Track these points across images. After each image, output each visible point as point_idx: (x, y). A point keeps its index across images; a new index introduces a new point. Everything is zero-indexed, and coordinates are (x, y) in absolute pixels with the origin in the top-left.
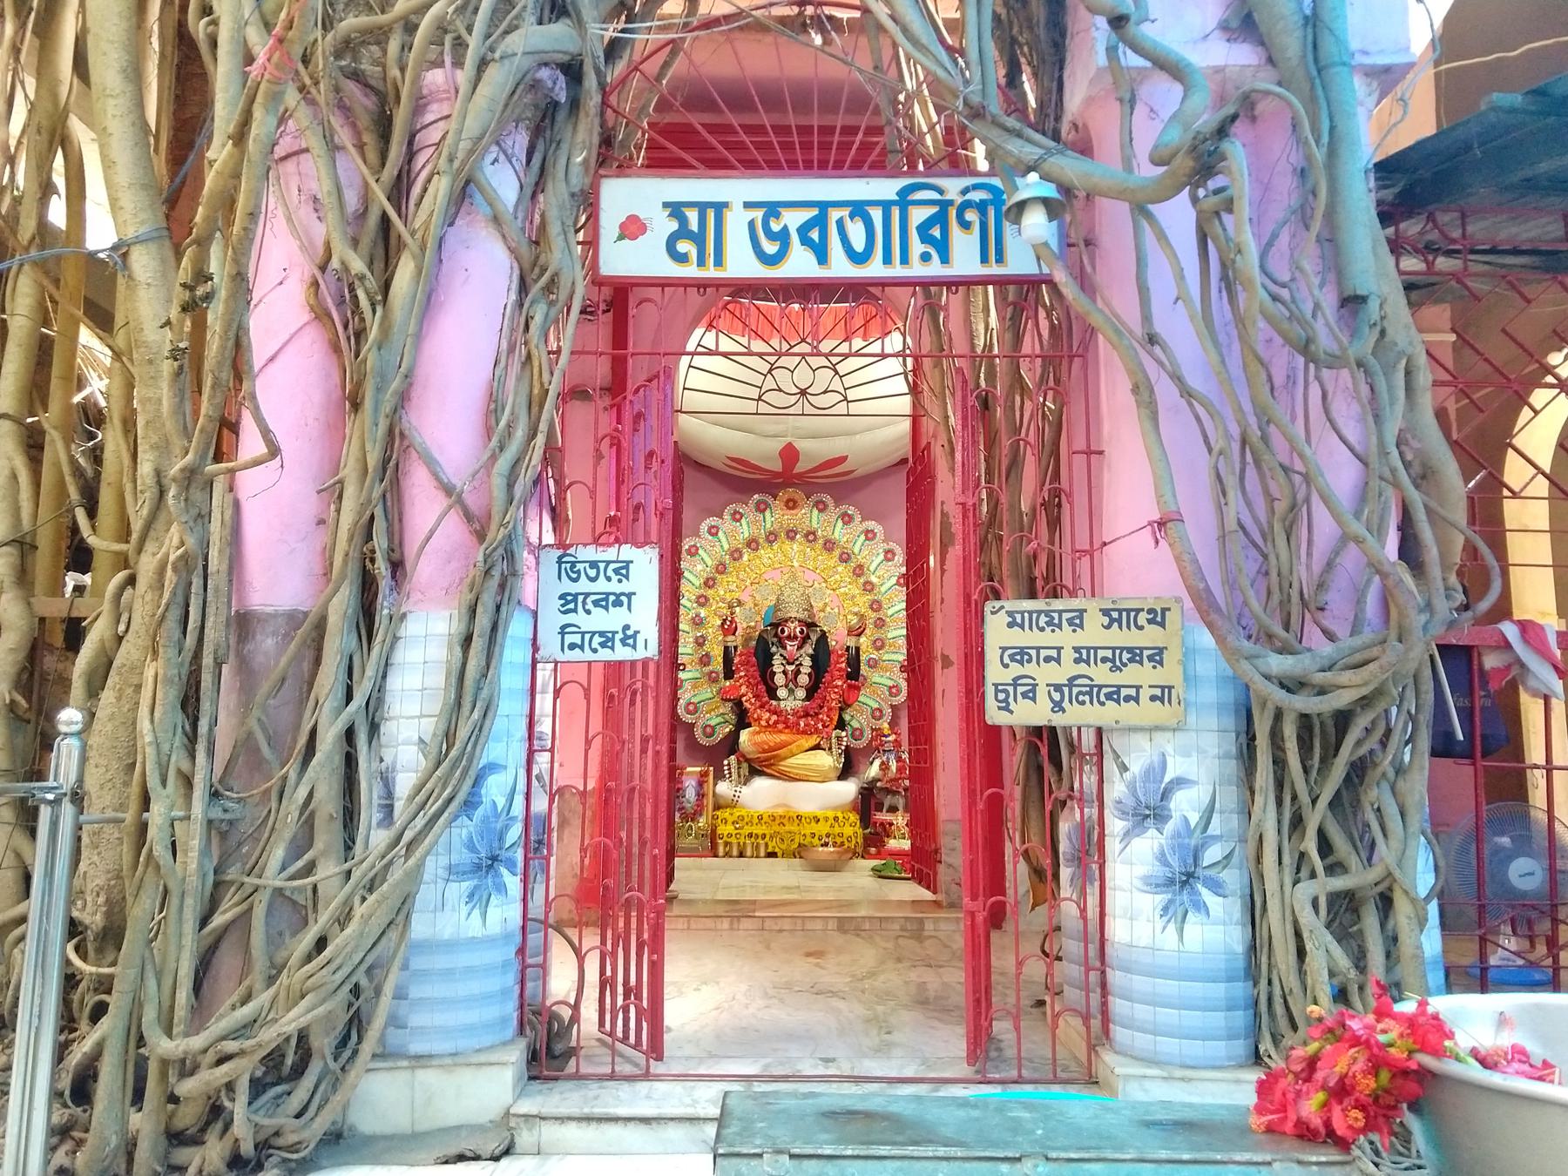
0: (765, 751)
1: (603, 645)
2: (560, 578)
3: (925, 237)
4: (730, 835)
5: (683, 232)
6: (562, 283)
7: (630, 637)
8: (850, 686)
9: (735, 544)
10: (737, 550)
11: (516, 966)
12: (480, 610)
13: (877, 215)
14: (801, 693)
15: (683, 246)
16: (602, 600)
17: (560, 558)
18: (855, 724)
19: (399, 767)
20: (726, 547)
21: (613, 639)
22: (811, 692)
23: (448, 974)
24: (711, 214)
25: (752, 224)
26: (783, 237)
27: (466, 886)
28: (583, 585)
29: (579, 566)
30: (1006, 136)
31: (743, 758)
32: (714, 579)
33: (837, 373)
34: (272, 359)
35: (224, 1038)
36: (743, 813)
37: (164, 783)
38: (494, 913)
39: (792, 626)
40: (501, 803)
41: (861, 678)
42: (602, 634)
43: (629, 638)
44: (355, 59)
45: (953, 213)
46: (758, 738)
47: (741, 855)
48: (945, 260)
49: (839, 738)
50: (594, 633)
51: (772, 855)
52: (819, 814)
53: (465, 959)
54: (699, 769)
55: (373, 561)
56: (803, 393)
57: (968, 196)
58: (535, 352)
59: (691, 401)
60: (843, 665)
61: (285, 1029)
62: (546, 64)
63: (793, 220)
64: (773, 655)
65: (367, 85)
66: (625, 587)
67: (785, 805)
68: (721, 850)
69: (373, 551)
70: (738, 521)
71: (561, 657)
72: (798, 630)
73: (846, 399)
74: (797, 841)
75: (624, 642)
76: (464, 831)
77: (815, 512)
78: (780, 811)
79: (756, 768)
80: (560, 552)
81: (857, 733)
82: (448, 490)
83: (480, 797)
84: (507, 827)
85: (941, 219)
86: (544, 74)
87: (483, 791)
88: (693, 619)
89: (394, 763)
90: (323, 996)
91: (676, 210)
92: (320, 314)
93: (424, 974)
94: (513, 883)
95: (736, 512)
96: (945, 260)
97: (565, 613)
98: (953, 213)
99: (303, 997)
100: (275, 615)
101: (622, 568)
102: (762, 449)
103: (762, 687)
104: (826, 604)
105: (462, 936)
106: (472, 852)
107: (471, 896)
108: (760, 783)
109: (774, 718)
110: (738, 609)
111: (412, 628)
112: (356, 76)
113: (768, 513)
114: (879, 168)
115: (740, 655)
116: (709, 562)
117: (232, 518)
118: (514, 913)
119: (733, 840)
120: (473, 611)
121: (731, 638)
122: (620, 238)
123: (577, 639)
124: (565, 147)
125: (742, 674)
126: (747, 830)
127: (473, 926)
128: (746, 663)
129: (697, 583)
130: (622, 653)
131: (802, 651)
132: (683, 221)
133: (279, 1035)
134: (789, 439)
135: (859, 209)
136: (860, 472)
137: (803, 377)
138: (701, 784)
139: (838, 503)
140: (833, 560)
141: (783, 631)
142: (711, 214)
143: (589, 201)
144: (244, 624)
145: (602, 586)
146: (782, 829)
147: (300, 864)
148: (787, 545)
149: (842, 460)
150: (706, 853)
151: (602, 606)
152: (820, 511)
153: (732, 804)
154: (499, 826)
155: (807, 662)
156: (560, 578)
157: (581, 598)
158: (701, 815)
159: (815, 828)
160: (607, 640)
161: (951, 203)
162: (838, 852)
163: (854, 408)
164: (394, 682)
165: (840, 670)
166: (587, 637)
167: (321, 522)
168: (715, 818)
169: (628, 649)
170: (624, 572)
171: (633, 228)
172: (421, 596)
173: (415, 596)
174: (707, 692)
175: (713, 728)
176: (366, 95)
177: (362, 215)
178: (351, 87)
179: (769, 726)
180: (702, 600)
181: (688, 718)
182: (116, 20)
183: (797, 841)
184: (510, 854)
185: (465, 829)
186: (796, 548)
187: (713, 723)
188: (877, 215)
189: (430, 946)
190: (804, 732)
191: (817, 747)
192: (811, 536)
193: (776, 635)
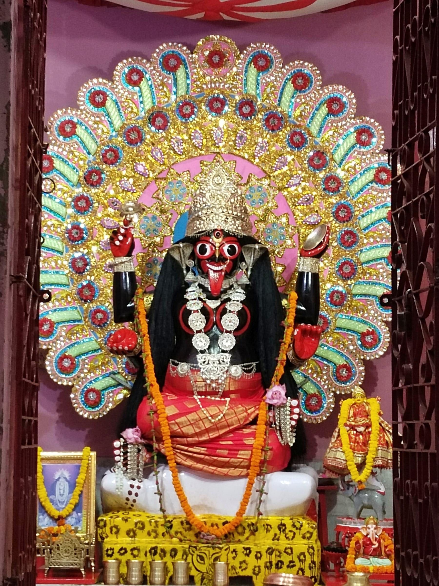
10: (135, 129)
20: (118, 123)
32: (99, 172)
64: (188, 285)
70: (136, 84)
72: (226, 247)
116: (92, 147)
131: (232, 280)
141: (203, 250)
180: (82, 204)
187: (98, 386)
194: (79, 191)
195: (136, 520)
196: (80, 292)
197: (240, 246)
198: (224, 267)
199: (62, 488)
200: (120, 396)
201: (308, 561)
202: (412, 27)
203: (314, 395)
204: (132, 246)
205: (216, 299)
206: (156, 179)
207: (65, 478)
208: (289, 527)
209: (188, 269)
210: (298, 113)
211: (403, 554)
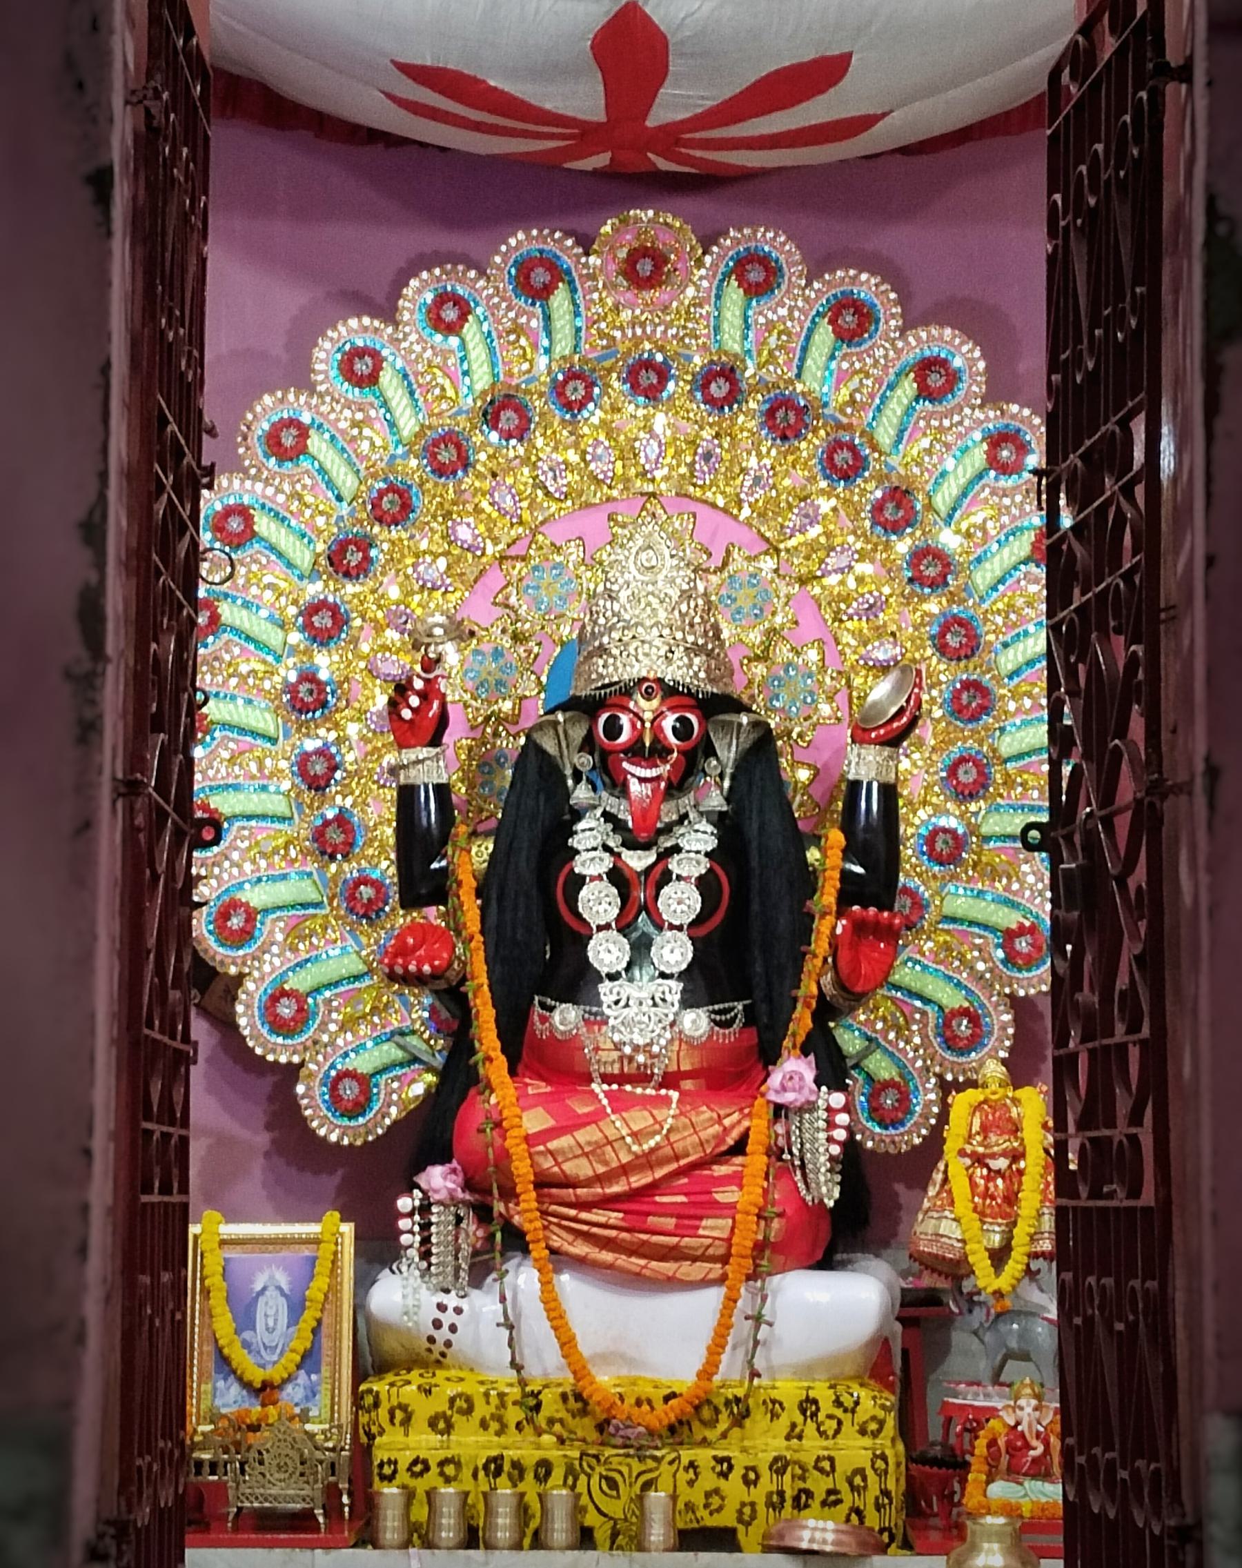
10: (451, 439)
20: (408, 425)
32: (365, 544)
47: (472, 1538)
64: (577, 815)
70: (451, 329)
72: (669, 722)
113: (560, 299)
116: (347, 481)
131: (686, 802)
141: (613, 729)
175: (364, 1081)
181: (281, 1050)
187: (363, 1063)
194: (314, 590)
195: (451, 1390)
196: (319, 835)
198: (663, 769)
199: (271, 1312)
200: (418, 1089)
202: (1088, 170)
204: (443, 721)
205: (646, 847)
207: (279, 1288)
208: (826, 1407)
209: (577, 776)
210: (844, 394)
211: (1081, 1460)
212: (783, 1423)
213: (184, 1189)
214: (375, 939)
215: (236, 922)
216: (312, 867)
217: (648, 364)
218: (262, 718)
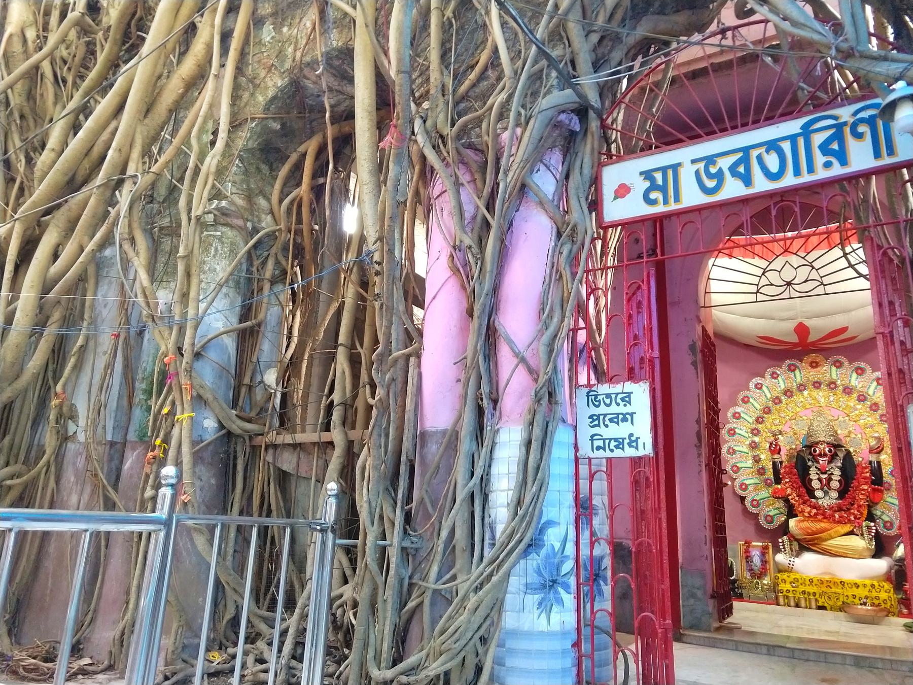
0: (809, 534)
1: (617, 447)
2: (588, 406)
3: (825, 148)
4: (788, 591)
5: (654, 187)
6: (579, 231)
7: (633, 441)
8: (874, 490)
9: (775, 394)
10: (777, 398)
11: (573, 654)
12: (535, 424)
13: (786, 146)
14: (835, 494)
15: (653, 195)
16: (615, 418)
17: (588, 393)
18: (886, 518)
19: (498, 520)
20: (769, 396)
21: (623, 443)
22: (842, 493)
23: (528, 653)
24: (670, 173)
25: (697, 173)
26: (720, 175)
27: (537, 597)
28: (603, 409)
29: (600, 397)
30: (874, 62)
31: (792, 538)
32: (762, 418)
33: (813, 268)
34: (434, 298)
35: (402, 674)
36: (798, 576)
37: (373, 524)
38: (556, 617)
39: (822, 447)
40: (557, 546)
41: (886, 485)
42: (616, 440)
43: (633, 442)
44: (469, 138)
45: (847, 130)
46: (804, 525)
47: (797, 605)
48: (844, 162)
49: (869, 527)
50: (610, 439)
51: (823, 608)
52: (858, 581)
53: (537, 645)
54: (761, 544)
55: (482, 399)
56: (789, 284)
57: (860, 115)
58: (564, 273)
59: (715, 299)
60: (868, 475)
61: (429, 674)
62: (563, 112)
63: (725, 163)
64: (810, 467)
65: (476, 149)
66: (629, 409)
67: (830, 574)
68: (781, 601)
69: (481, 395)
70: (776, 378)
71: (592, 455)
72: (827, 449)
73: (822, 284)
74: (841, 599)
75: (630, 445)
76: (535, 562)
77: (834, 368)
78: (827, 577)
79: (805, 545)
80: (587, 390)
81: (888, 525)
82: (523, 360)
83: (544, 541)
84: (562, 562)
85: (839, 136)
86: (563, 117)
87: (545, 538)
88: (750, 444)
89: (496, 518)
90: (450, 656)
91: (647, 175)
92: (455, 270)
93: (511, 651)
94: (569, 600)
95: (774, 373)
96: (844, 162)
97: (592, 427)
98: (847, 130)
99: (441, 655)
100: (436, 432)
101: (626, 397)
102: (783, 330)
103: (803, 490)
104: (850, 432)
105: (536, 629)
106: (540, 576)
107: (540, 604)
108: (808, 557)
109: (814, 511)
110: (780, 436)
111: (502, 437)
112: (471, 146)
113: (797, 372)
114: (788, 115)
115: (785, 468)
116: (758, 407)
117: (417, 382)
118: (570, 619)
119: (790, 595)
120: (531, 424)
121: (776, 456)
122: (615, 198)
123: (601, 443)
124: (580, 155)
125: (787, 480)
126: (802, 588)
127: (542, 624)
128: (789, 473)
129: (751, 421)
130: (630, 452)
131: (833, 465)
132: (652, 180)
133: (426, 676)
134: (800, 320)
135: (772, 145)
136: (861, 338)
137: (788, 275)
138: (763, 554)
139: (851, 362)
140: (852, 402)
141: (815, 451)
142: (670, 173)
143: (596, 181)
144: (422, 438)
145: (614, 409)
146: (828, 590)
147: (448, 576)
148: (815, 393)
149: (844, 330)
150: (770, 601)
151: (614, 422)
152: (837, 367)
153: (788, 570)
154: (556, 561)
155: (837, 472)
156: (588, 406)
157: (602, 417)
158: (766, 575)
159: (855, 591)
160: (620, 443)
161: (845, 123)
162: (874, 610)
163: (829, 289)
164: (495, 470)
165: (865, 478)
166: (607, 441)
167: (459, 380)
168: (777, 578)
169: (633, 450)
170: (627, 399)
171: (622, 191)
172: (507, 419)
173: (504, 418)
174: (764, 493)
175: (772, 517)
176: (476, 155)
177: (474, 218)
178: (469, 153)
179: (811, 516)
180: (755, 432)
181: (754, 510)
182: (367, 149)
183: (841, 599)
184: (565, 579)
185: (535, 560)
186: (821, 395)
187: (771, 514)
188: (786, 146)
189: (515, 634)
190: (839, 522)
191: (851, 533)
192: (832, 385)
193: (810, 454)
194: (754, 426)
195: (794, 577)
196: (758, 471)
197: (835, 449)
200: (783, 519)
201: (889, 604)
203: (888, 522)
204: (780, 450)
205: (825, 473)
206: (790, 419)
208: (877, 586)
209: (809, 460)
210: (860, 385)
212: (867, 589)
213: (725, 534)
214: (771, 490)
215: (744, 487)
216: (757, 476)
217: (817, 382)
218: (745, 449)
